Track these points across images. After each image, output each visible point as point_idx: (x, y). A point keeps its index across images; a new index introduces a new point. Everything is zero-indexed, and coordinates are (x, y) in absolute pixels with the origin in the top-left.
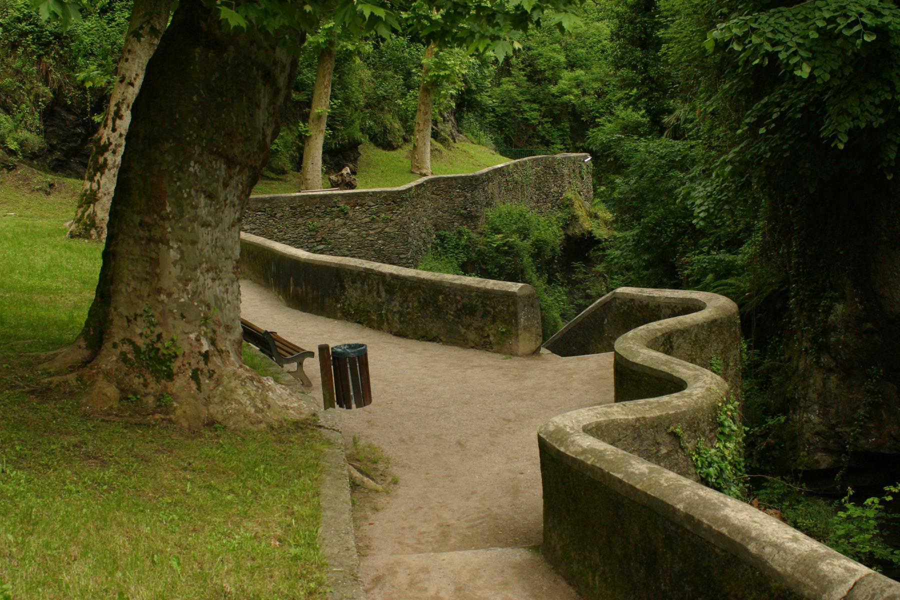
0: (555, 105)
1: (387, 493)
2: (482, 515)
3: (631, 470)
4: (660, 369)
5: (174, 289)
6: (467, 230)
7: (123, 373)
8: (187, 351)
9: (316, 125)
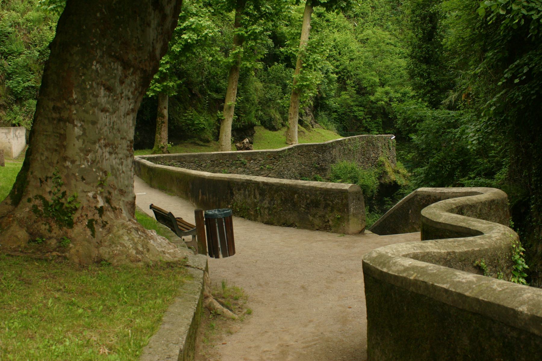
0: (373, 108)
1: (242, 321)
2: (316, 338)
3: (457, 280)
4: (459, 225)
5: (77, 158)
6: (320, 177)
7: (33, 221)
8: (85, 206)
9: (228, 112)
